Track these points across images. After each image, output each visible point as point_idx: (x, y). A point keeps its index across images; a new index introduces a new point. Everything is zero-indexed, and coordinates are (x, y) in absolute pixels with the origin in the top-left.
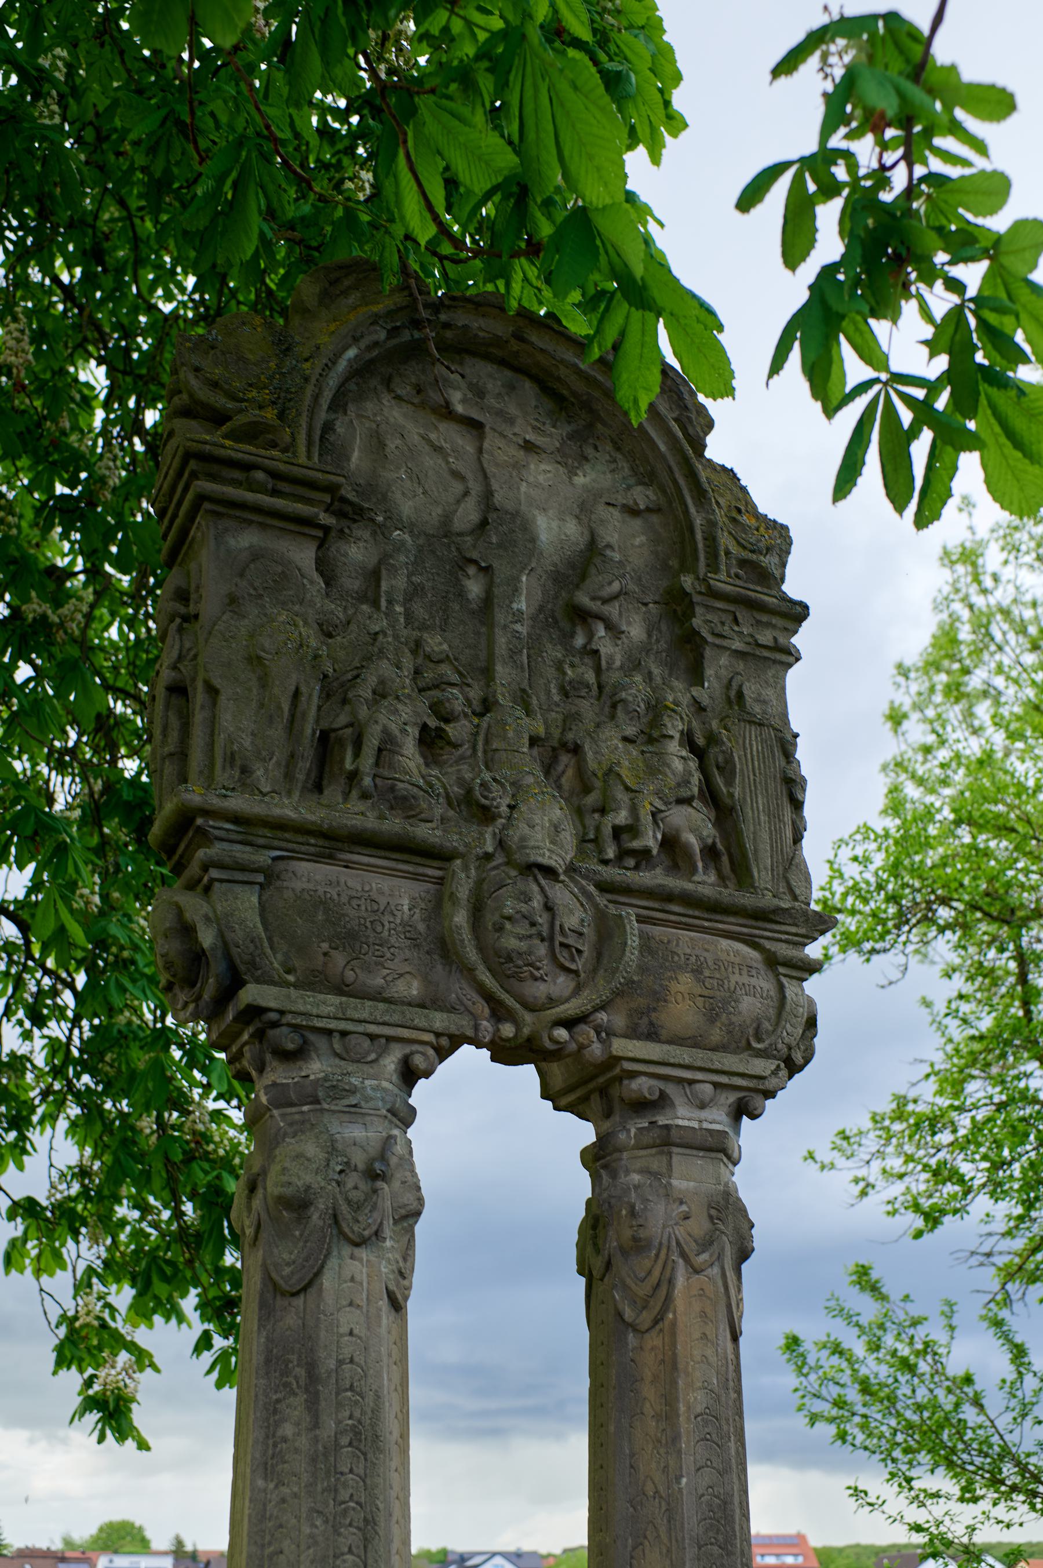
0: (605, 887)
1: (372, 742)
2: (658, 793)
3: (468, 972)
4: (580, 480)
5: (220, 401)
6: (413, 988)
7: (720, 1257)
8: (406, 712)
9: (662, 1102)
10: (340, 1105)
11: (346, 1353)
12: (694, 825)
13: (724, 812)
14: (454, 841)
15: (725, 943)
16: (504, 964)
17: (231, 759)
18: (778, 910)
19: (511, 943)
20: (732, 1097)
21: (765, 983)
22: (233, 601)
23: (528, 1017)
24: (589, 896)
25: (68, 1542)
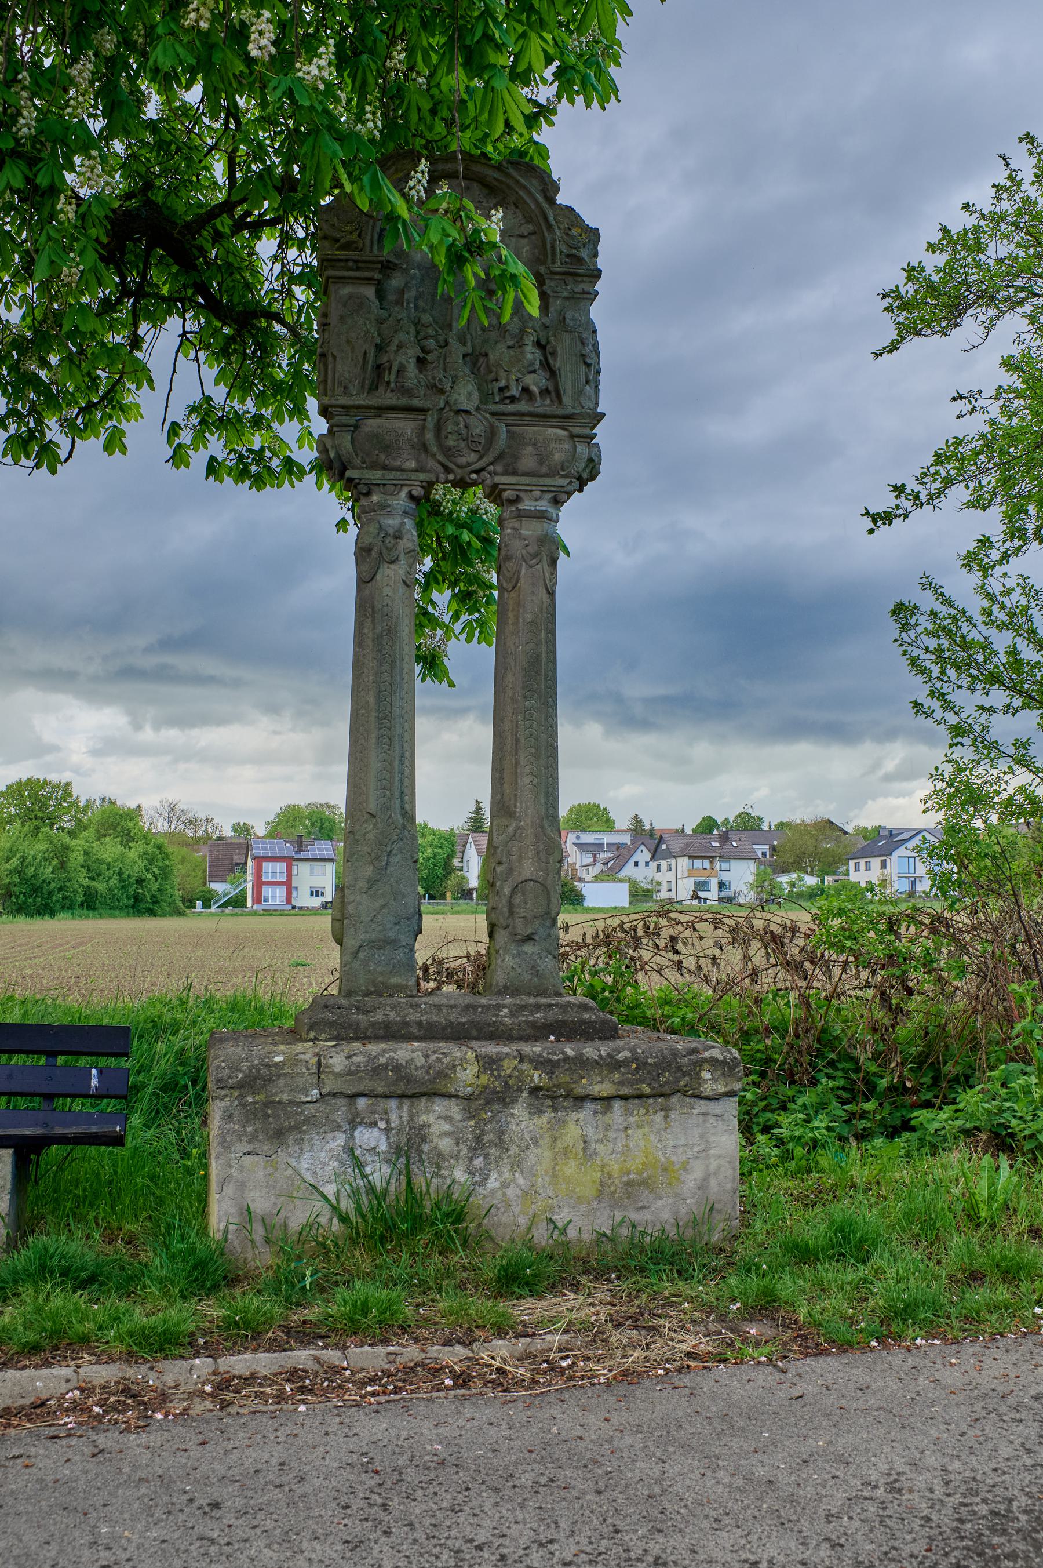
0: (493, 414)
1: (395, 369)
2: (519, 371)
3: (433, 456)
6: (413, 465)
9: (518, 500)
12: (536, 382)
14: (428, 404)
15: (550, 430)
17: (340, 383)
20: (550, 495)
21: (567, 446)
23: (459, 471)
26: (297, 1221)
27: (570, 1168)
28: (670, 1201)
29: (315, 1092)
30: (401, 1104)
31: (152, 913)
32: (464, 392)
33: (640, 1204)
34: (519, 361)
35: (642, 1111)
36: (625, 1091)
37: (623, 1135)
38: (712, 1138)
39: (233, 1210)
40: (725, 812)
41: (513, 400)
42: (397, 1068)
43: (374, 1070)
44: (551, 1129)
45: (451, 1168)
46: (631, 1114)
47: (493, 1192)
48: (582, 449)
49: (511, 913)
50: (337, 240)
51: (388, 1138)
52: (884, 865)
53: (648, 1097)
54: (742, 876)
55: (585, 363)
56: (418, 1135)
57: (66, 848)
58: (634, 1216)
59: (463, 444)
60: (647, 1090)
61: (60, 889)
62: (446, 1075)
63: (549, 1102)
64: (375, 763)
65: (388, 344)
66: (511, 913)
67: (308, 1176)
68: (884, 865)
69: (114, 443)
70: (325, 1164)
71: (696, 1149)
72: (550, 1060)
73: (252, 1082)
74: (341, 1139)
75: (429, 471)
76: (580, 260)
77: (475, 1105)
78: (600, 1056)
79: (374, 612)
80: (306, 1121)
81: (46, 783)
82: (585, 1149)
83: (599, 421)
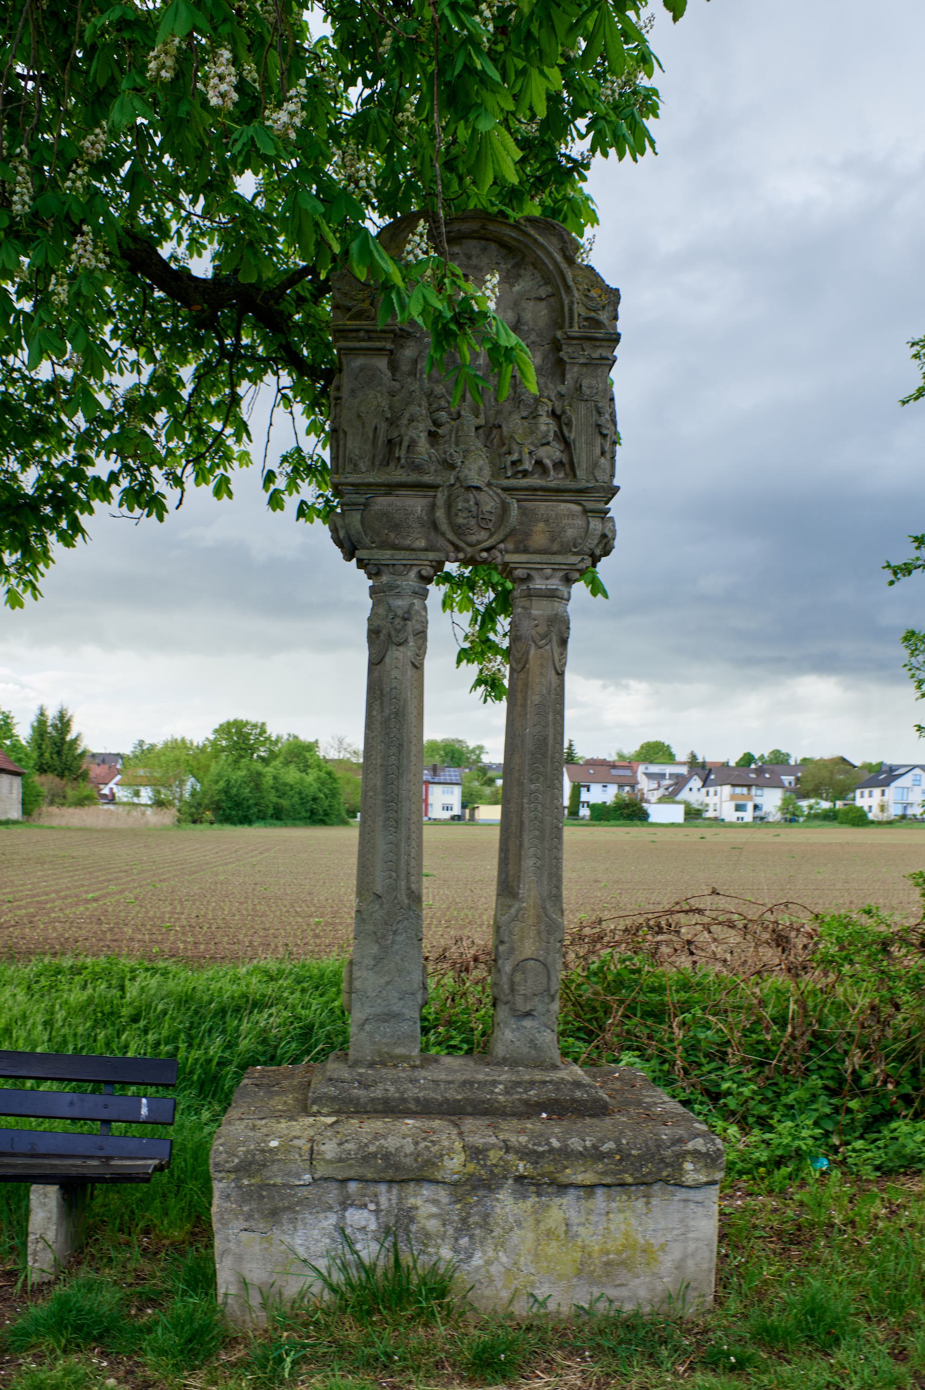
0: (505, 489)
1: (405, 444)
3: (443, 534)
4: (516, 288)
5: (349, 303)
6: (422, 543)
7: (550, 641)
8: (421, 426)
9: (529, 578)
10: (393, 593)
11: (394, 685)
12: (551, 453)
13: (567, 445)
14: (439, 480)
16: (458, 530)
17: (351, 460)
18: (587, 488)
19: (460, 521)
20: (562, 573)
21: (580, 522)
22: (353, 391)
23: (469, 549)
24: (498, 495)
25: (621, 756)
26: (292, 1290)
27: (552, 1248)
28: (648, 1279)
29: (307, 1177)
30: (390, 1187)
31: (323, 822)
32: (474, 467)
33: (618, 1282)
34: (532, 432)
35: (624, 1197)
36: (608, 1180)
37: (604, 1218)
38: (692, 1223)
39: (232, 1279)
40: (762, 750)
41: (525, 474)
42: (387, 1156)
43: (363, 1158)
44: (535, 1212)
45: (438, 1247)
46: (614, 1201)
47: (478, 1269)
48: (595, 524)
49: (512, 990)
50: (349, 310)
51: (378, 1219)
52: (883, 794)
53: (630, 1185)
54: (771, 800)
55: (601, 433)
56: (407, 1216)
57: (259, 774)
58: (611, 1292)
59: (473, 522)
60: (630, 1180)
61: (256, 804)
62: (434, 1164)
63: (533, 1188)
64: (381, 847)
65: (399, 418)
66: (512, 990)
67: (301, 1252)
68: (883, 794)
69: (223, 488)
70: (317, 1241)
71: (675, 1232)
72: (536, 1152)
73: (245, 1168)
74: (332, 1219)
75: (438, 550)
76: (598, 324)
77: (460, 1191)
78: (585, 1148)
79: (382, 695)
80: (299, 1203)
81: (247, 723)
82: (566, 1232)
83: (614, 495)
